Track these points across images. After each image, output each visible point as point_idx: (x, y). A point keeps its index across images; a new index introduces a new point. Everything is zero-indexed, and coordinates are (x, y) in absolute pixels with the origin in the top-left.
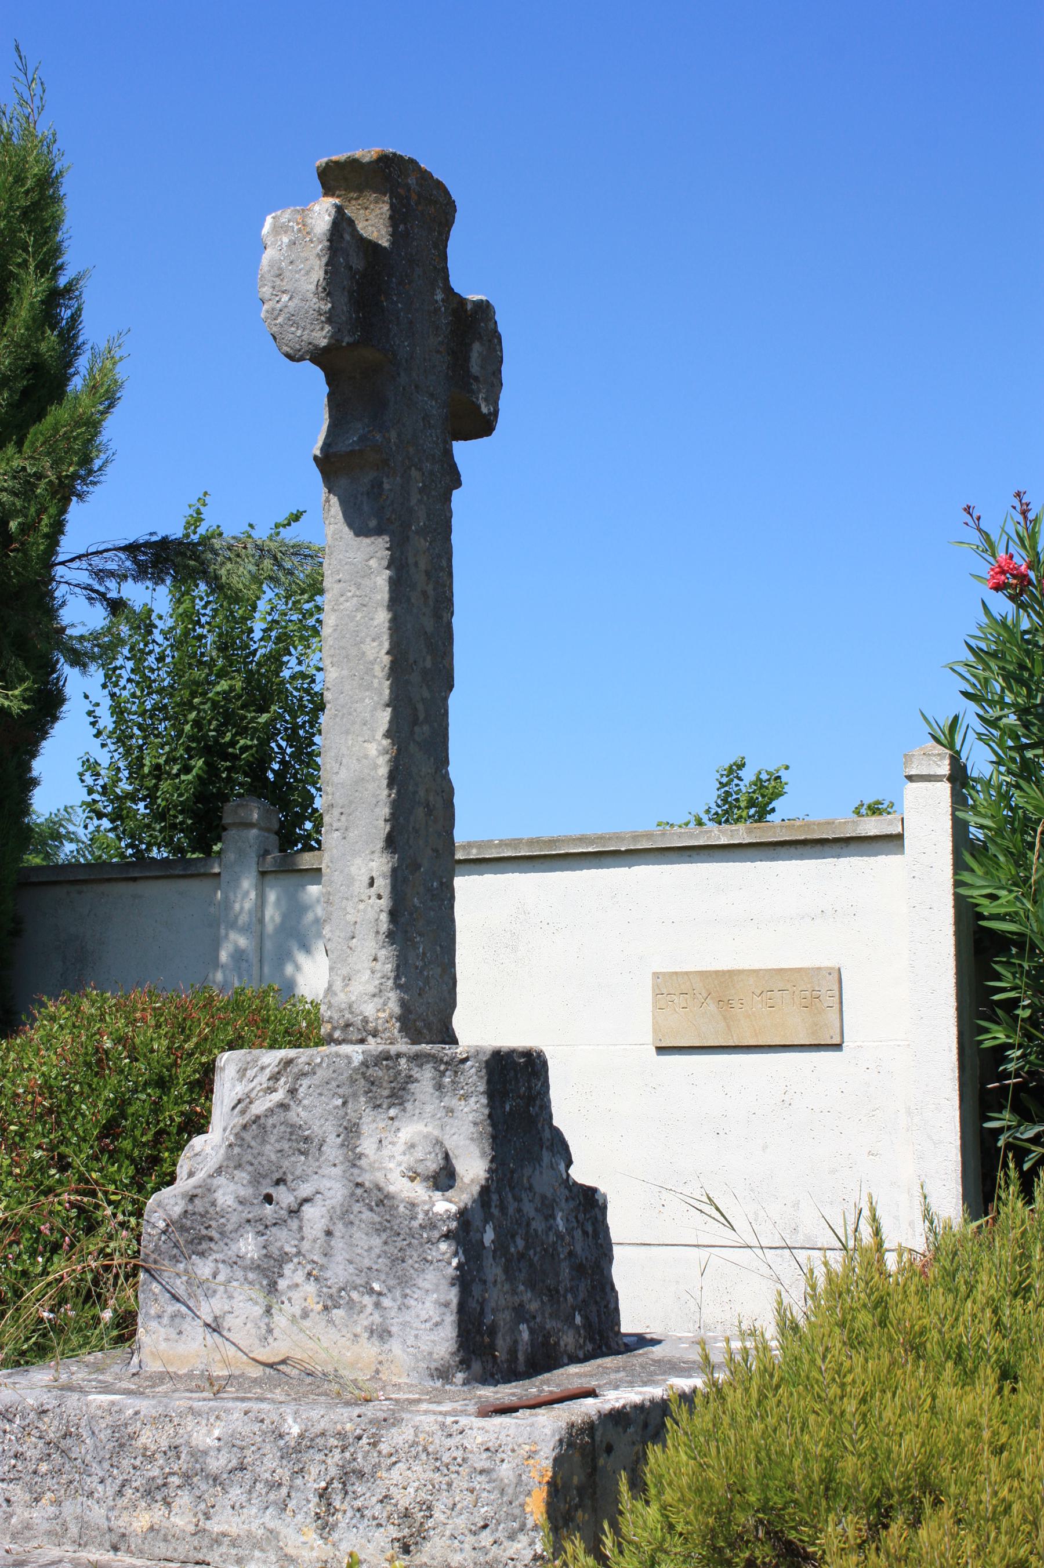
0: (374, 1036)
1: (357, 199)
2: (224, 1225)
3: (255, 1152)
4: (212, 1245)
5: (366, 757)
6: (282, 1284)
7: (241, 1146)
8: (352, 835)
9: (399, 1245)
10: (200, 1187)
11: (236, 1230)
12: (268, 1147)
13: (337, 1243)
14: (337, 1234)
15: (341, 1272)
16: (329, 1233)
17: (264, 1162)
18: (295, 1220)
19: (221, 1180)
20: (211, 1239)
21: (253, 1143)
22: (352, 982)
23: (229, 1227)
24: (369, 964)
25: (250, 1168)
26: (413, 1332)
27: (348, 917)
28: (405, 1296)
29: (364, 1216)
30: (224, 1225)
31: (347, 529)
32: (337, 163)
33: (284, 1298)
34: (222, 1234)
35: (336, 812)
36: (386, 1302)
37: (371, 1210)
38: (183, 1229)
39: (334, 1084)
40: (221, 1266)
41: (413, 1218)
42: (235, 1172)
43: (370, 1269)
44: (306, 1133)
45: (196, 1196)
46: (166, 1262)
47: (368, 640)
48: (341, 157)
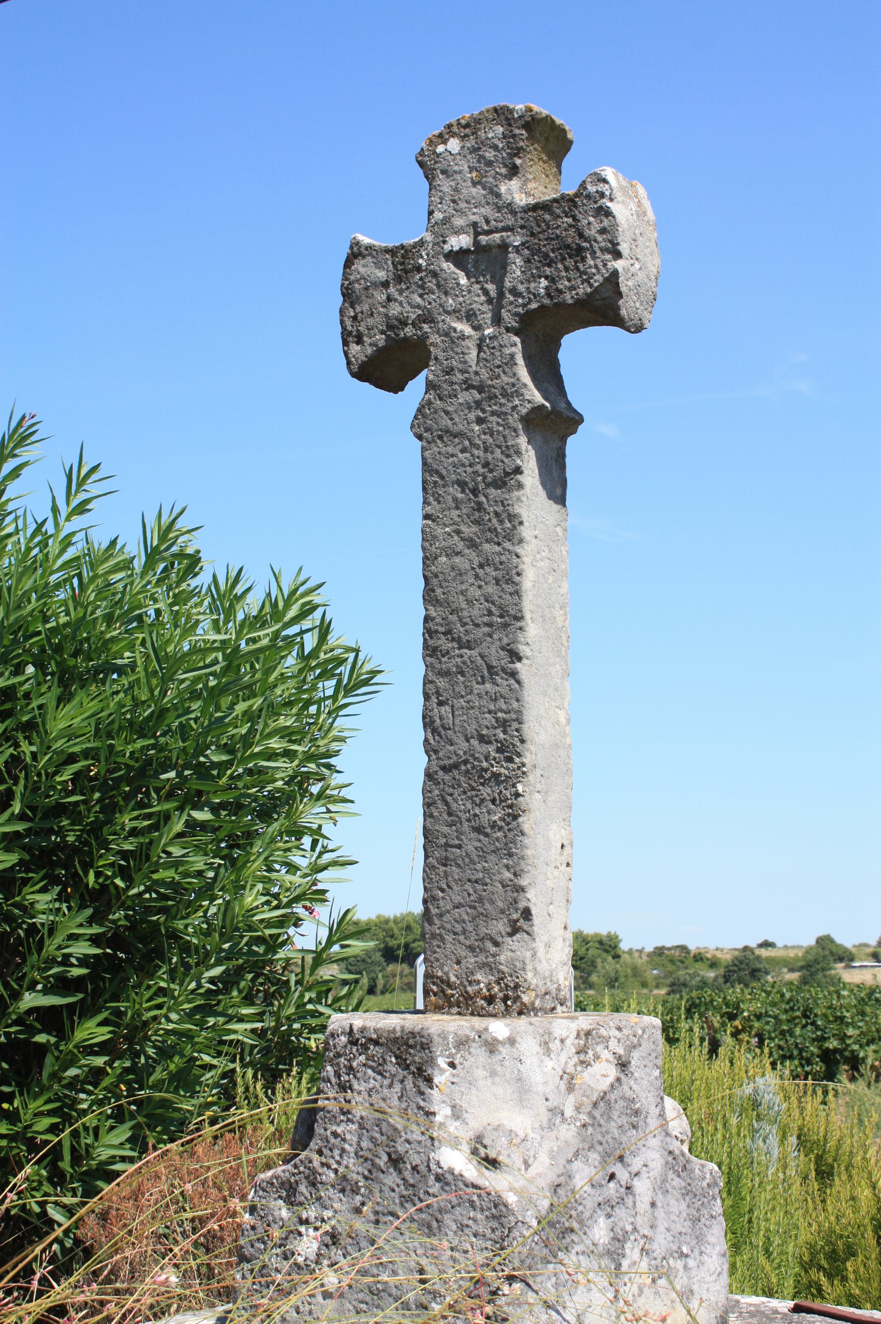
0: (562, 1005)
1: (544, 162)
2: (582, 1212)
3: (604, 1129)
4: (574, 1237)
5: (558, 723)
6: (625, 1263)
7: (593, 1125)
8: (551, 798)
9: (696, 1205)
10: (562, 1174)
11: (591, 1217)
12: (613, 1124)
13: (660, 1213)
14: (659, 1204)
15: (662, 1242)
16: (653, 1204)
17: (610, 1140)
18: (630, 1196)
19: (577, 1165)
20: (572, 1230)
21: (602, 1122)
22: (551, 950)
23: (587, 1214)
24: (561, 931)
25: (600, 1148)
26: (706, 1286)
27: (548, 882)
28: (701, 1253)
29: (674, 1183)
30: (582, 1212)
31: (540, 487)
32: (553, 121)
33: (626, 1280)
34: (581, 1222)
35: (538, 772)
36: (691, 1263)
37: (679, 1176)
38: (551, 1224)
39: (654, 1055)
40: (581, 1257)
41: (704, 1178)
42: (589, 1154)
43: (680, 1233)
44: (637, 1106)
45: (559, 1185)
46: (539, 1266)
47: (557, 606)
48: (558, 121)
